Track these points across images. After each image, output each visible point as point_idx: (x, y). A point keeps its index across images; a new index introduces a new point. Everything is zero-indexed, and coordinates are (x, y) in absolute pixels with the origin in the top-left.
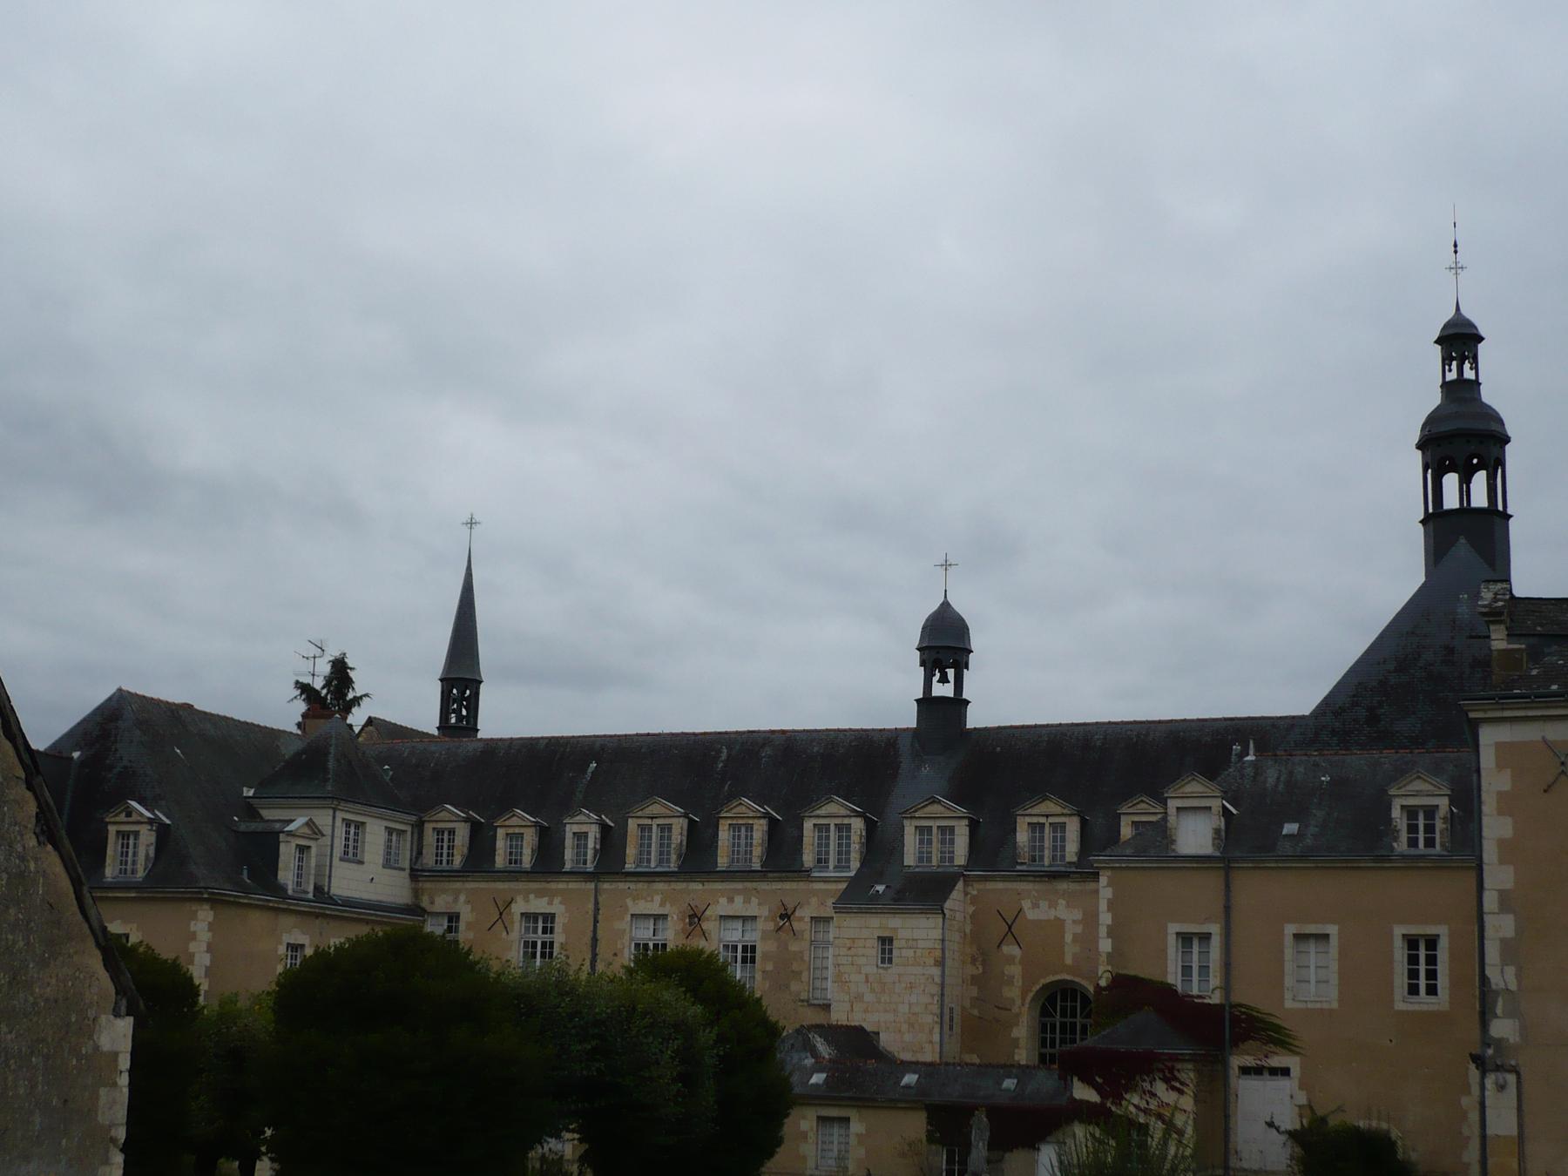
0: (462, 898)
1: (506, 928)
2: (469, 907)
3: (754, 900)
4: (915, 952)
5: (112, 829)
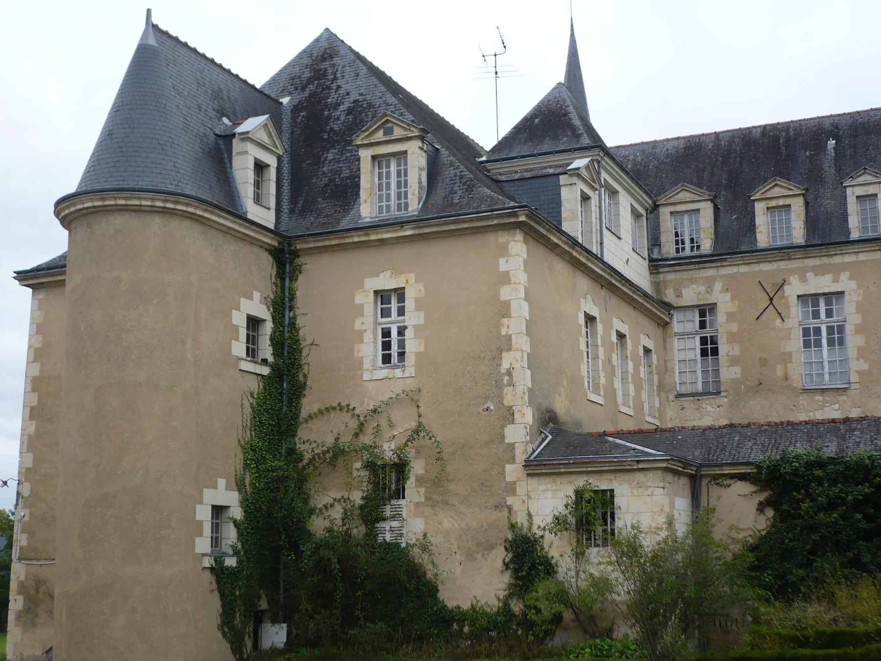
0: (718, 286)
1: (780, 314)
2: (728, 296)
3: (810, 275)
5: (365, 155)
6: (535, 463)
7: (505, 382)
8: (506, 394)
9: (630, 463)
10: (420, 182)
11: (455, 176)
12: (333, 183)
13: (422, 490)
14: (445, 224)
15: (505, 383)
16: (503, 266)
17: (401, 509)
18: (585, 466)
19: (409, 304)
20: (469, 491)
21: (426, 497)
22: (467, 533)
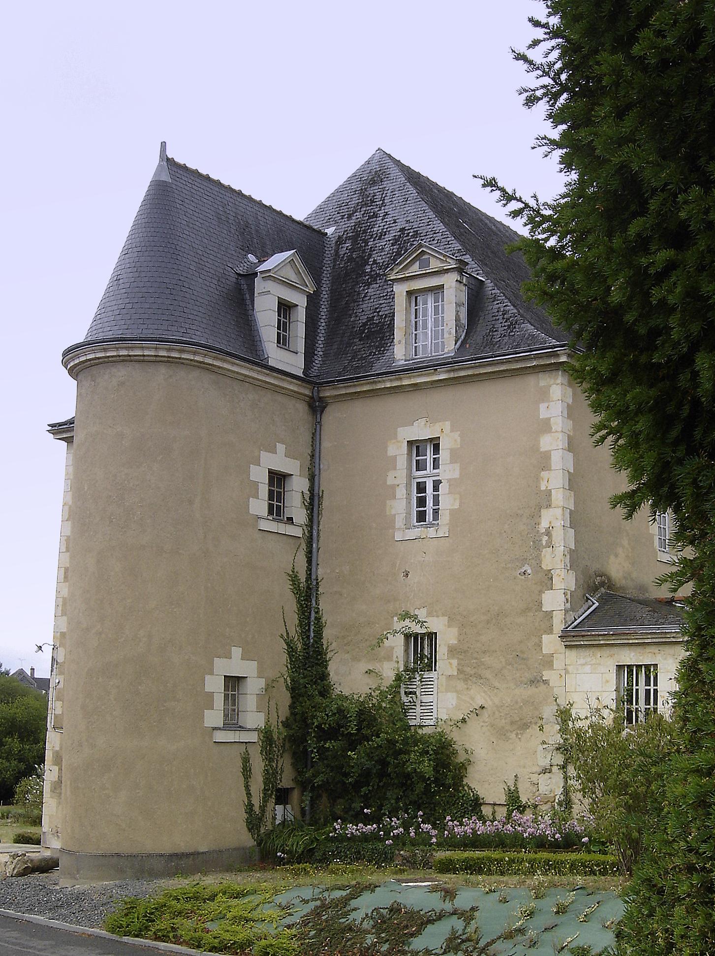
5: (400, 290)
6: (573, 634)
7: (544, 543)
8: (545, 556)
9: (674, 635)
10: (457, 319)
11: (498, 311)
12: (371, 322)
13: (455, 662)
14: (482, 366)
15: (544, 544)
16: (543, 413)
17: (432, 683)
18: (626, 637)
19: (444, 455)
20: (504, 663)
21: (458, 670)
22: (501, 710)
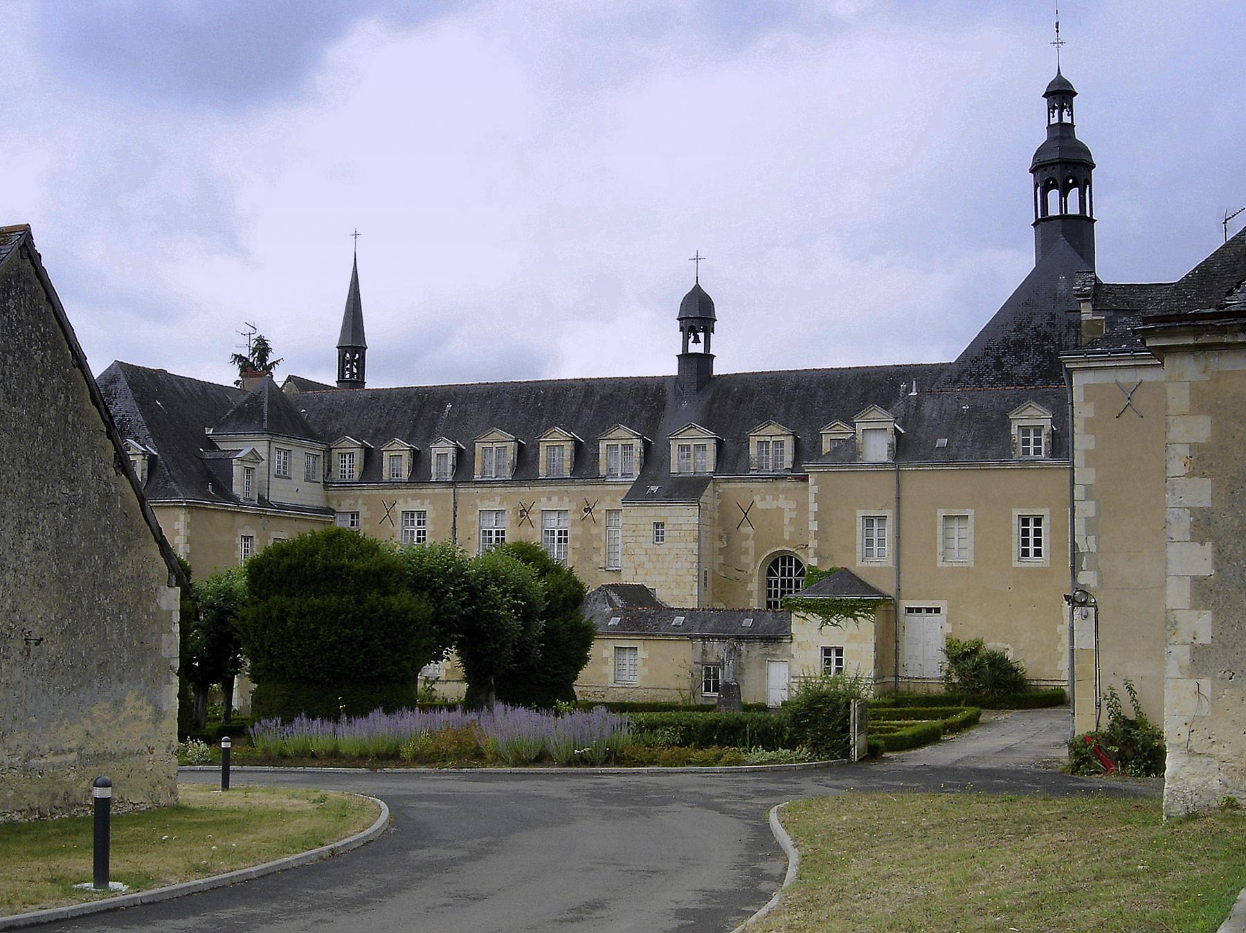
0: (360, 502)
2: (366, 507)
3: (566, 499)
4: (680, 533)
